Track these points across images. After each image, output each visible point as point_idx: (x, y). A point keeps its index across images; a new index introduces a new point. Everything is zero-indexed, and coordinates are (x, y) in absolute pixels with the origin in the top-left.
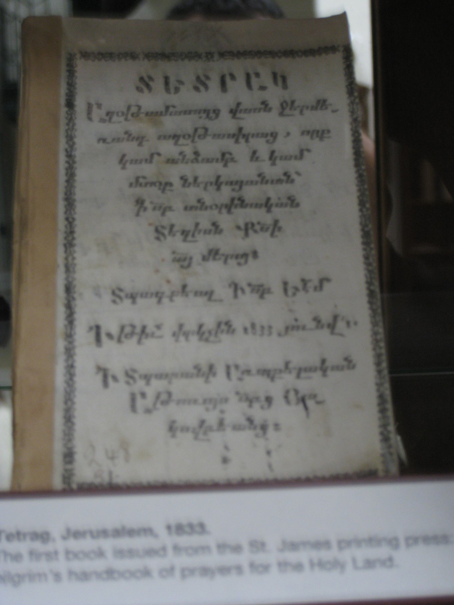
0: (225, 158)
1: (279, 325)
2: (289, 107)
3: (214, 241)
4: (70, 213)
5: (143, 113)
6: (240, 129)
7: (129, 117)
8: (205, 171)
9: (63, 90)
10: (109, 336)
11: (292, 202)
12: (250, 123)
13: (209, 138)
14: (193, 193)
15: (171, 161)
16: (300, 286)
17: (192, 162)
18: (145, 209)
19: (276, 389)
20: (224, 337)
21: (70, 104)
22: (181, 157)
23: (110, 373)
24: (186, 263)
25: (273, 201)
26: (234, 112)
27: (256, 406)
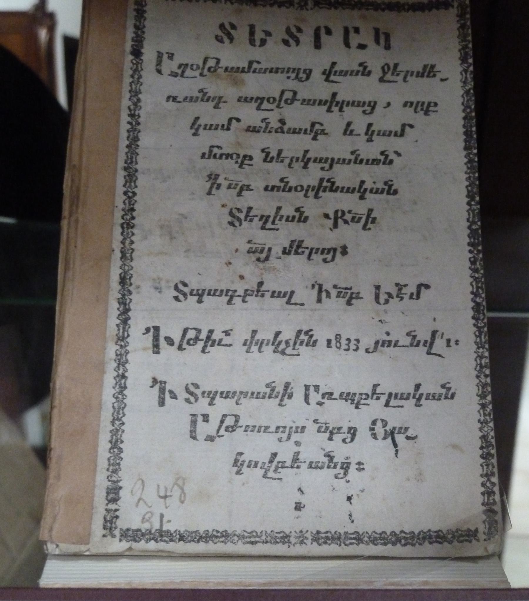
0: (316, 131)
1: (367, 342)
2: (390, 73)
3: (297, 231)
4: (130, 187)
5: (222, 67)
6: (334, 95)
7: (206, 72)
8: (293, 145)
9: (130, 34)
10: (170, 341)
11: (390, 189)
12: (348, 89)
13: (297, 104)
14: (278, 170)
15: (252, 130)
16: (394, 291)
17: (276, 132)
18: (219, 186)
19: (361, 418)
20: (303, 349)
21: (137, 53)
22: (263, 125)
23: (168, 387)
24: (263, 256)
25: (368, 185)
26: (327, 75)
27: (338, 438)
